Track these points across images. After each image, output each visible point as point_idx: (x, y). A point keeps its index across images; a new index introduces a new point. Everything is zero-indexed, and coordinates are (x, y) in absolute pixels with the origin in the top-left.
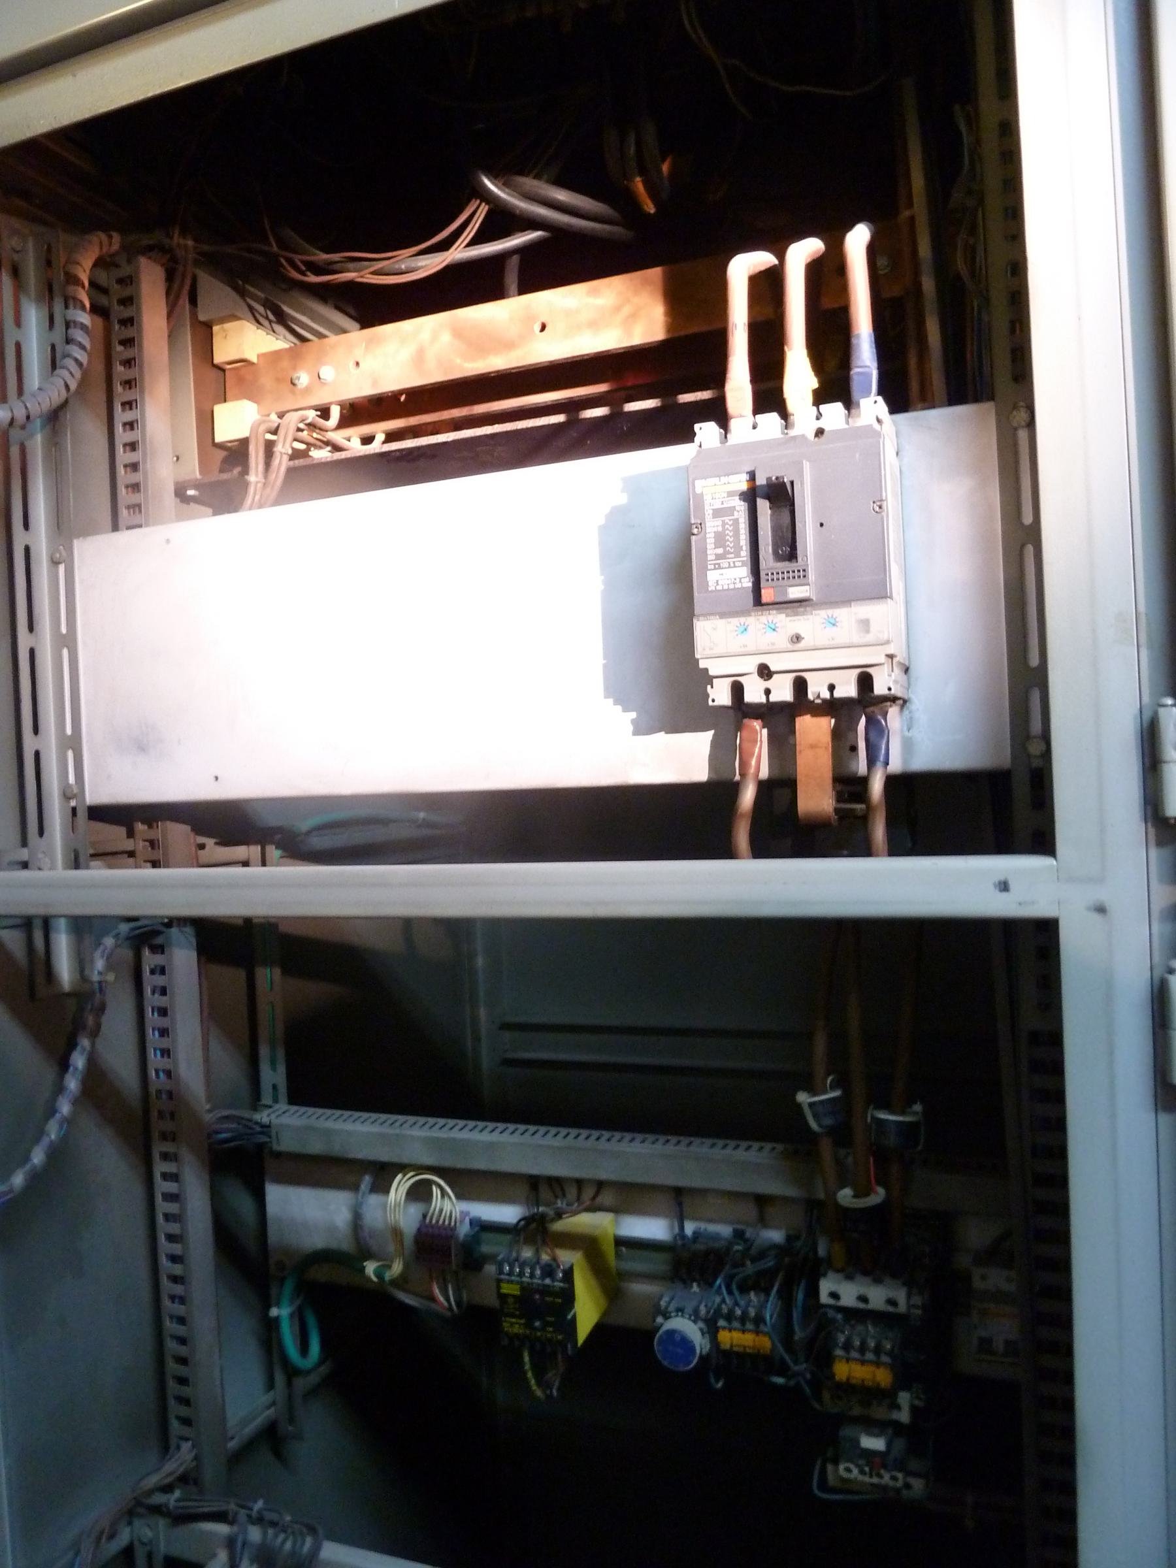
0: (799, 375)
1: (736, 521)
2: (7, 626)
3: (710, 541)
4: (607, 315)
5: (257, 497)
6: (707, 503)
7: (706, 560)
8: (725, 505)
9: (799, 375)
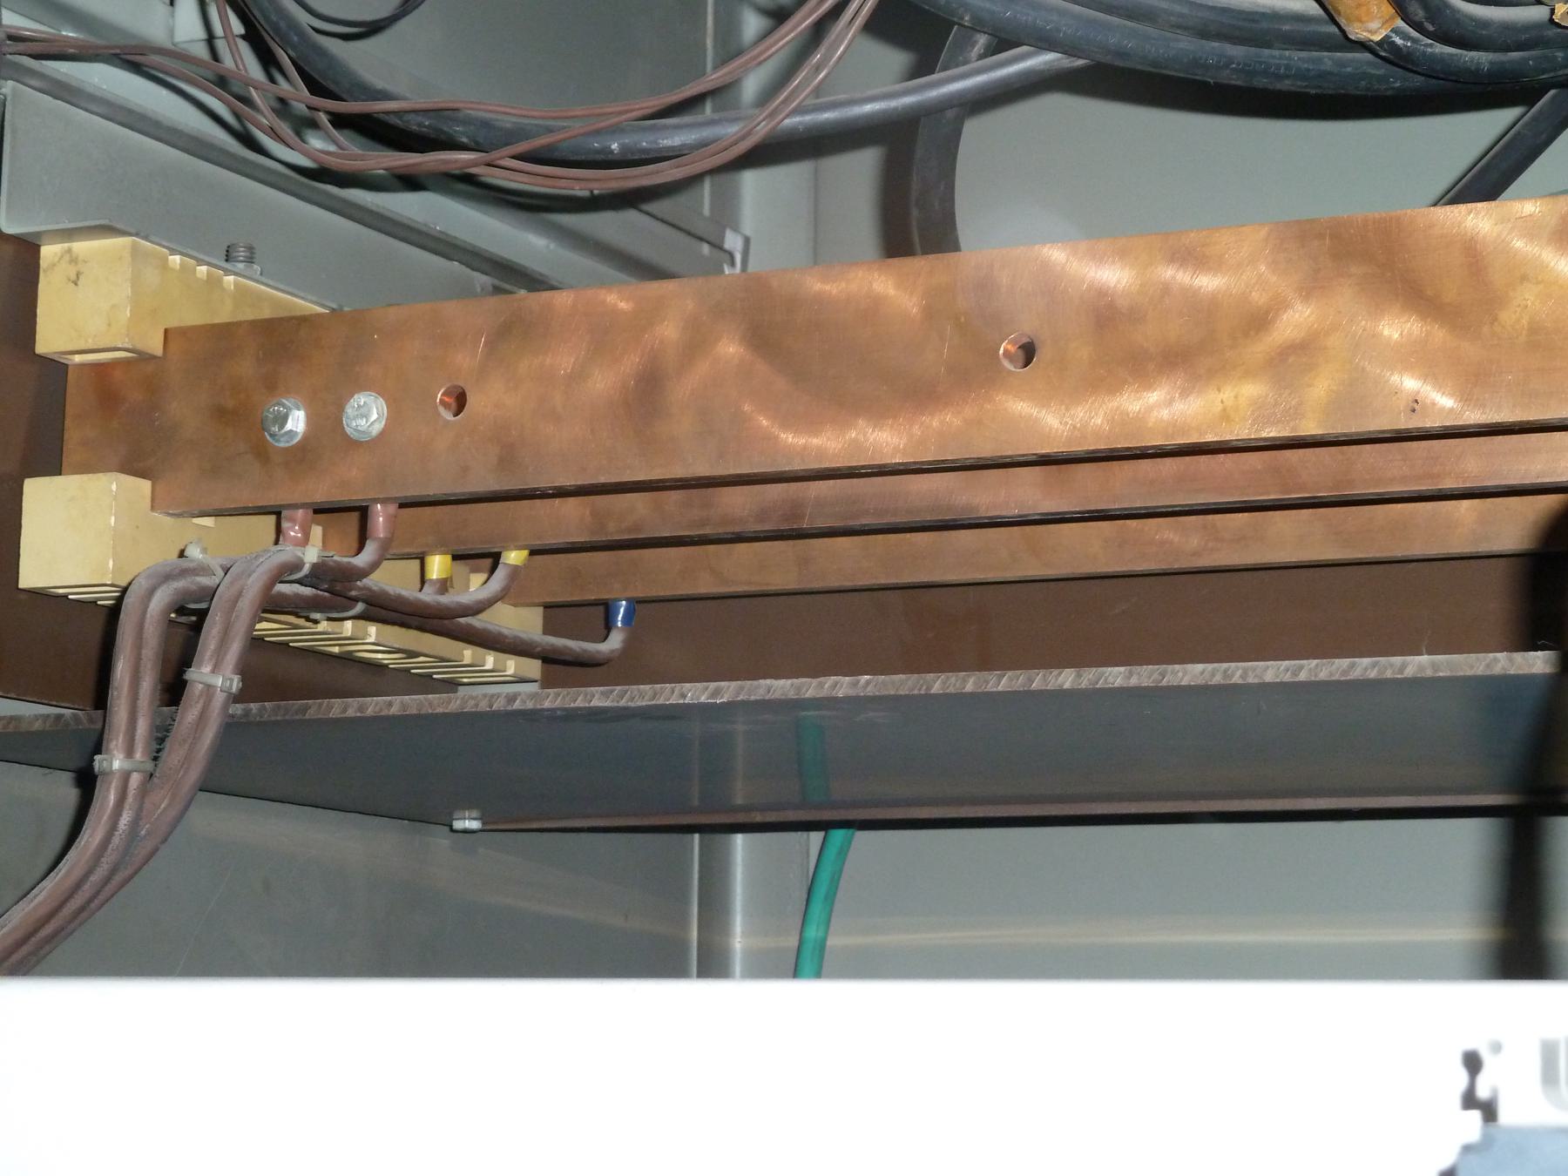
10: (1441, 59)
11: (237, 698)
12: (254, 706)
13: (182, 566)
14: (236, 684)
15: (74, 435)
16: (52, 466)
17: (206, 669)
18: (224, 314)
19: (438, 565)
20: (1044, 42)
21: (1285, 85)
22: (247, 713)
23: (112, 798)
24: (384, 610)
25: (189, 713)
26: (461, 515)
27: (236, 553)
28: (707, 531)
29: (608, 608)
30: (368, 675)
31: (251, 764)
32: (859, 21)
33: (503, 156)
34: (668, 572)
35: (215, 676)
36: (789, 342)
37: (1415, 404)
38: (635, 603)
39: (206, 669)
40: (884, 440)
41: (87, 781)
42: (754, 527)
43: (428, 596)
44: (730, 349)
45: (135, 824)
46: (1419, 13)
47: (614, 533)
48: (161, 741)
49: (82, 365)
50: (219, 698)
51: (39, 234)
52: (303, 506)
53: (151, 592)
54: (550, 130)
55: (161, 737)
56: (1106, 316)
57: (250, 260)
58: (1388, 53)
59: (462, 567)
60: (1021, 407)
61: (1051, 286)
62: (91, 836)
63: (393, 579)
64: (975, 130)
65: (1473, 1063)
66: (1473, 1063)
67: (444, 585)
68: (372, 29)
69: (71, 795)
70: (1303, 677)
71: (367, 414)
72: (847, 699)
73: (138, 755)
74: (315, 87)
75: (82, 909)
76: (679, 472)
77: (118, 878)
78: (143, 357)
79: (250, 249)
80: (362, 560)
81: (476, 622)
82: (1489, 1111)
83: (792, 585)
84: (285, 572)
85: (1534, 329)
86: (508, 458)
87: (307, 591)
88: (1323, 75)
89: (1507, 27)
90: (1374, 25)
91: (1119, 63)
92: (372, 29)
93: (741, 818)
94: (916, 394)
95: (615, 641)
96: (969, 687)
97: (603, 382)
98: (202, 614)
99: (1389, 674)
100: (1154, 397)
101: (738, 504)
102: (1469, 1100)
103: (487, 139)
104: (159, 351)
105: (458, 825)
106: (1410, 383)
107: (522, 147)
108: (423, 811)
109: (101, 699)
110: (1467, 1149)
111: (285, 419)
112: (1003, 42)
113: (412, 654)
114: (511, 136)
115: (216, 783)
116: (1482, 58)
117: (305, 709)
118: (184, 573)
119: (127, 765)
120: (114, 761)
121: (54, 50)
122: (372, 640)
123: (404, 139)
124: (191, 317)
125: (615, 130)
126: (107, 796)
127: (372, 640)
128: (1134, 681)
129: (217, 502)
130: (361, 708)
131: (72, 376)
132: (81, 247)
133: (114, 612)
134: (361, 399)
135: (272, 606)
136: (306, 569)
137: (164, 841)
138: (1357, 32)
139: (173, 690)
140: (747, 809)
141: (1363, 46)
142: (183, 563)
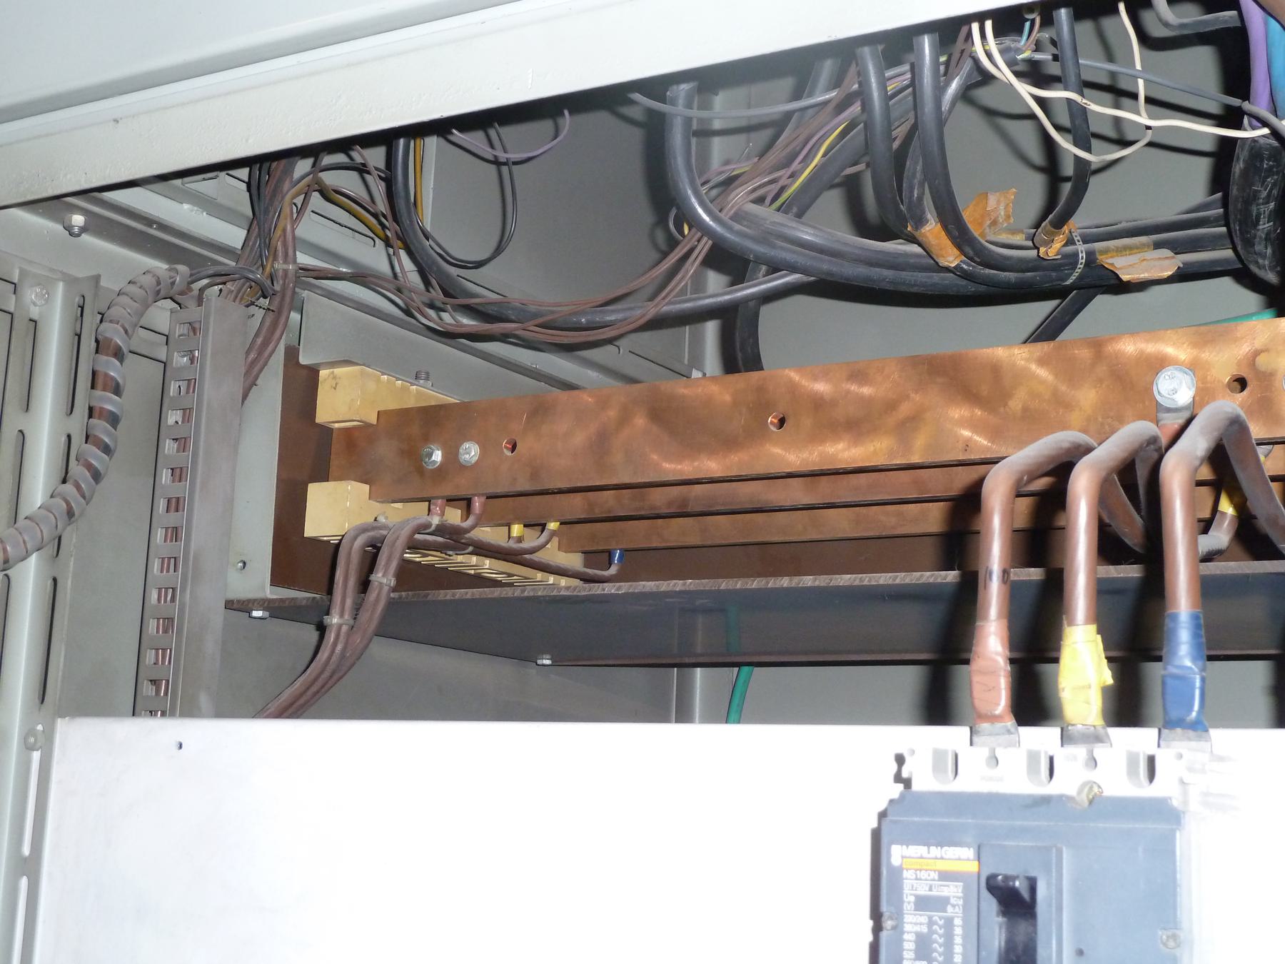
0: (1083, 664)
1: (949, 923)
2: (478, 161)
3: (909, 945)
4: (1028, 24)
5: (339, 647)
6: (907, 885)
7: (901, 949)
8: (934, 893)
9: (1083, 664)
10: (988, 276)
11: (394, 590)
12: (404, 594)
13: (375, 525)
14: (393, 583)
15: (335, 463)
16: (323, 476)
17: (380, 575)
18: (411, 403)
19: (517, 529)
20: (793, 269)
21: (915, 290)
22: (400, 597)
23: (333, 636)
24: (483, 550)
25: (372, 595)
26: (525, 501)
27: (400, 516)
28: (643, 513)
29: (610, 554)
30: (479, 580)
31: (399, 624)
32: (700, 258)
33: (530, 325)
34: (638, 534)
35: (383, 578)
36: (672, 420)
37: (967, 446)
38: (625, 552)
39: (380, 575)
40: (712, 466)
41: (322, 629)
42: (664, 511)
43: (513, 545)
44: (640, 421)
45: (345, 649)
46: (971, 253)
47: (598, 513)
48: (358, 610)
49: (339, 429)
50: (386, 589)
51: (319, 365)
52: (442, 498)
53: (355, 538)
54: (553, 312)
55: (357, 609)
56: (818, 404)
57: (427, 379)
58: (956, 271)
59: (528, 530)
60: (777, 450)
61: (793, 389)
62: (323, 655)
63: (487, 534)
64: (766, 311)
65: (900, 760)
66: (900, 760)
67: (520, 540)
68: (479, 265)
69: (315, 635)
70: (898, 581)
71: (470, 452)
72: (681, 592)
73: (346, 617)
74: (446, 294)
75: (318, 692)
76: (615, 481)
77: (335, 677)
78: (367, 425)
79: (427, 373)
80: (466, 524)
81: (536, 557)
82: (907, 783)
83: (699, 543)
84: (422, 528)
85: (1025, 409)
86: (534, 475)
87: (440, 539)
88: (934, 285)
89: (1021, 260)
90: (951, 259)
91: (829, 278)
92: (479, 265)
93: (701, 660)
94: (729, 443)
95: (613, 570)
96: (739, 586)
97: (580, 439)
98: (378, 549)
99: (939, 580)
100: (841, 446)
101: (659, 498)
102: (898, 778)
103: (523, 315)
104: (374, 421)
105: (539, 662)
106: (966, 433)
107: (540, 320)
108: (523, 655)
109: (330, 591)
110: (891, 801)
111: (431, 455)
112: (774, 268)
113: (510, 575)
114: (535, 315)
115: (384, 631)
116: (1011, 276)
117: (426, 596)
118: (374, 528)
119: (341, 621)
120: (334, 620)
121: (322, 275)
122: (488, 566)
123: (493, 321)
124: (392, 405)
125: (583, 313)
126: (331, 637)
127: (488, 566)
128: (817, 583)
129: (411, 494)
130: (454, 595)
131: (334, 435)
132: (339, 371)
133: (338, 546)
134: (466, 445)
135: (414, 546)
136: (433, 528)
137: (359, 658)
138: (943, 262)
139: (364, 585)
140: (702, 655)
141: (947, 269)
142: (375, 524)
